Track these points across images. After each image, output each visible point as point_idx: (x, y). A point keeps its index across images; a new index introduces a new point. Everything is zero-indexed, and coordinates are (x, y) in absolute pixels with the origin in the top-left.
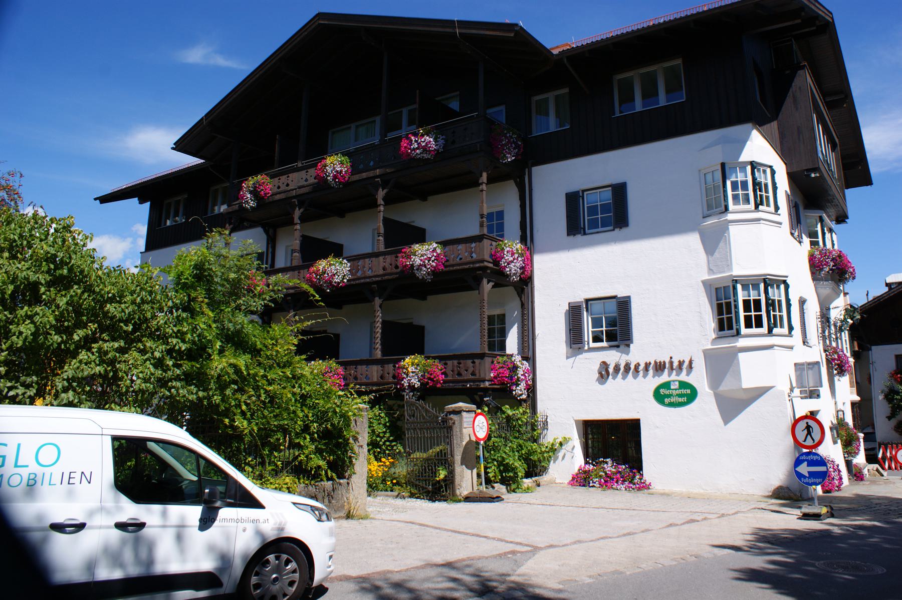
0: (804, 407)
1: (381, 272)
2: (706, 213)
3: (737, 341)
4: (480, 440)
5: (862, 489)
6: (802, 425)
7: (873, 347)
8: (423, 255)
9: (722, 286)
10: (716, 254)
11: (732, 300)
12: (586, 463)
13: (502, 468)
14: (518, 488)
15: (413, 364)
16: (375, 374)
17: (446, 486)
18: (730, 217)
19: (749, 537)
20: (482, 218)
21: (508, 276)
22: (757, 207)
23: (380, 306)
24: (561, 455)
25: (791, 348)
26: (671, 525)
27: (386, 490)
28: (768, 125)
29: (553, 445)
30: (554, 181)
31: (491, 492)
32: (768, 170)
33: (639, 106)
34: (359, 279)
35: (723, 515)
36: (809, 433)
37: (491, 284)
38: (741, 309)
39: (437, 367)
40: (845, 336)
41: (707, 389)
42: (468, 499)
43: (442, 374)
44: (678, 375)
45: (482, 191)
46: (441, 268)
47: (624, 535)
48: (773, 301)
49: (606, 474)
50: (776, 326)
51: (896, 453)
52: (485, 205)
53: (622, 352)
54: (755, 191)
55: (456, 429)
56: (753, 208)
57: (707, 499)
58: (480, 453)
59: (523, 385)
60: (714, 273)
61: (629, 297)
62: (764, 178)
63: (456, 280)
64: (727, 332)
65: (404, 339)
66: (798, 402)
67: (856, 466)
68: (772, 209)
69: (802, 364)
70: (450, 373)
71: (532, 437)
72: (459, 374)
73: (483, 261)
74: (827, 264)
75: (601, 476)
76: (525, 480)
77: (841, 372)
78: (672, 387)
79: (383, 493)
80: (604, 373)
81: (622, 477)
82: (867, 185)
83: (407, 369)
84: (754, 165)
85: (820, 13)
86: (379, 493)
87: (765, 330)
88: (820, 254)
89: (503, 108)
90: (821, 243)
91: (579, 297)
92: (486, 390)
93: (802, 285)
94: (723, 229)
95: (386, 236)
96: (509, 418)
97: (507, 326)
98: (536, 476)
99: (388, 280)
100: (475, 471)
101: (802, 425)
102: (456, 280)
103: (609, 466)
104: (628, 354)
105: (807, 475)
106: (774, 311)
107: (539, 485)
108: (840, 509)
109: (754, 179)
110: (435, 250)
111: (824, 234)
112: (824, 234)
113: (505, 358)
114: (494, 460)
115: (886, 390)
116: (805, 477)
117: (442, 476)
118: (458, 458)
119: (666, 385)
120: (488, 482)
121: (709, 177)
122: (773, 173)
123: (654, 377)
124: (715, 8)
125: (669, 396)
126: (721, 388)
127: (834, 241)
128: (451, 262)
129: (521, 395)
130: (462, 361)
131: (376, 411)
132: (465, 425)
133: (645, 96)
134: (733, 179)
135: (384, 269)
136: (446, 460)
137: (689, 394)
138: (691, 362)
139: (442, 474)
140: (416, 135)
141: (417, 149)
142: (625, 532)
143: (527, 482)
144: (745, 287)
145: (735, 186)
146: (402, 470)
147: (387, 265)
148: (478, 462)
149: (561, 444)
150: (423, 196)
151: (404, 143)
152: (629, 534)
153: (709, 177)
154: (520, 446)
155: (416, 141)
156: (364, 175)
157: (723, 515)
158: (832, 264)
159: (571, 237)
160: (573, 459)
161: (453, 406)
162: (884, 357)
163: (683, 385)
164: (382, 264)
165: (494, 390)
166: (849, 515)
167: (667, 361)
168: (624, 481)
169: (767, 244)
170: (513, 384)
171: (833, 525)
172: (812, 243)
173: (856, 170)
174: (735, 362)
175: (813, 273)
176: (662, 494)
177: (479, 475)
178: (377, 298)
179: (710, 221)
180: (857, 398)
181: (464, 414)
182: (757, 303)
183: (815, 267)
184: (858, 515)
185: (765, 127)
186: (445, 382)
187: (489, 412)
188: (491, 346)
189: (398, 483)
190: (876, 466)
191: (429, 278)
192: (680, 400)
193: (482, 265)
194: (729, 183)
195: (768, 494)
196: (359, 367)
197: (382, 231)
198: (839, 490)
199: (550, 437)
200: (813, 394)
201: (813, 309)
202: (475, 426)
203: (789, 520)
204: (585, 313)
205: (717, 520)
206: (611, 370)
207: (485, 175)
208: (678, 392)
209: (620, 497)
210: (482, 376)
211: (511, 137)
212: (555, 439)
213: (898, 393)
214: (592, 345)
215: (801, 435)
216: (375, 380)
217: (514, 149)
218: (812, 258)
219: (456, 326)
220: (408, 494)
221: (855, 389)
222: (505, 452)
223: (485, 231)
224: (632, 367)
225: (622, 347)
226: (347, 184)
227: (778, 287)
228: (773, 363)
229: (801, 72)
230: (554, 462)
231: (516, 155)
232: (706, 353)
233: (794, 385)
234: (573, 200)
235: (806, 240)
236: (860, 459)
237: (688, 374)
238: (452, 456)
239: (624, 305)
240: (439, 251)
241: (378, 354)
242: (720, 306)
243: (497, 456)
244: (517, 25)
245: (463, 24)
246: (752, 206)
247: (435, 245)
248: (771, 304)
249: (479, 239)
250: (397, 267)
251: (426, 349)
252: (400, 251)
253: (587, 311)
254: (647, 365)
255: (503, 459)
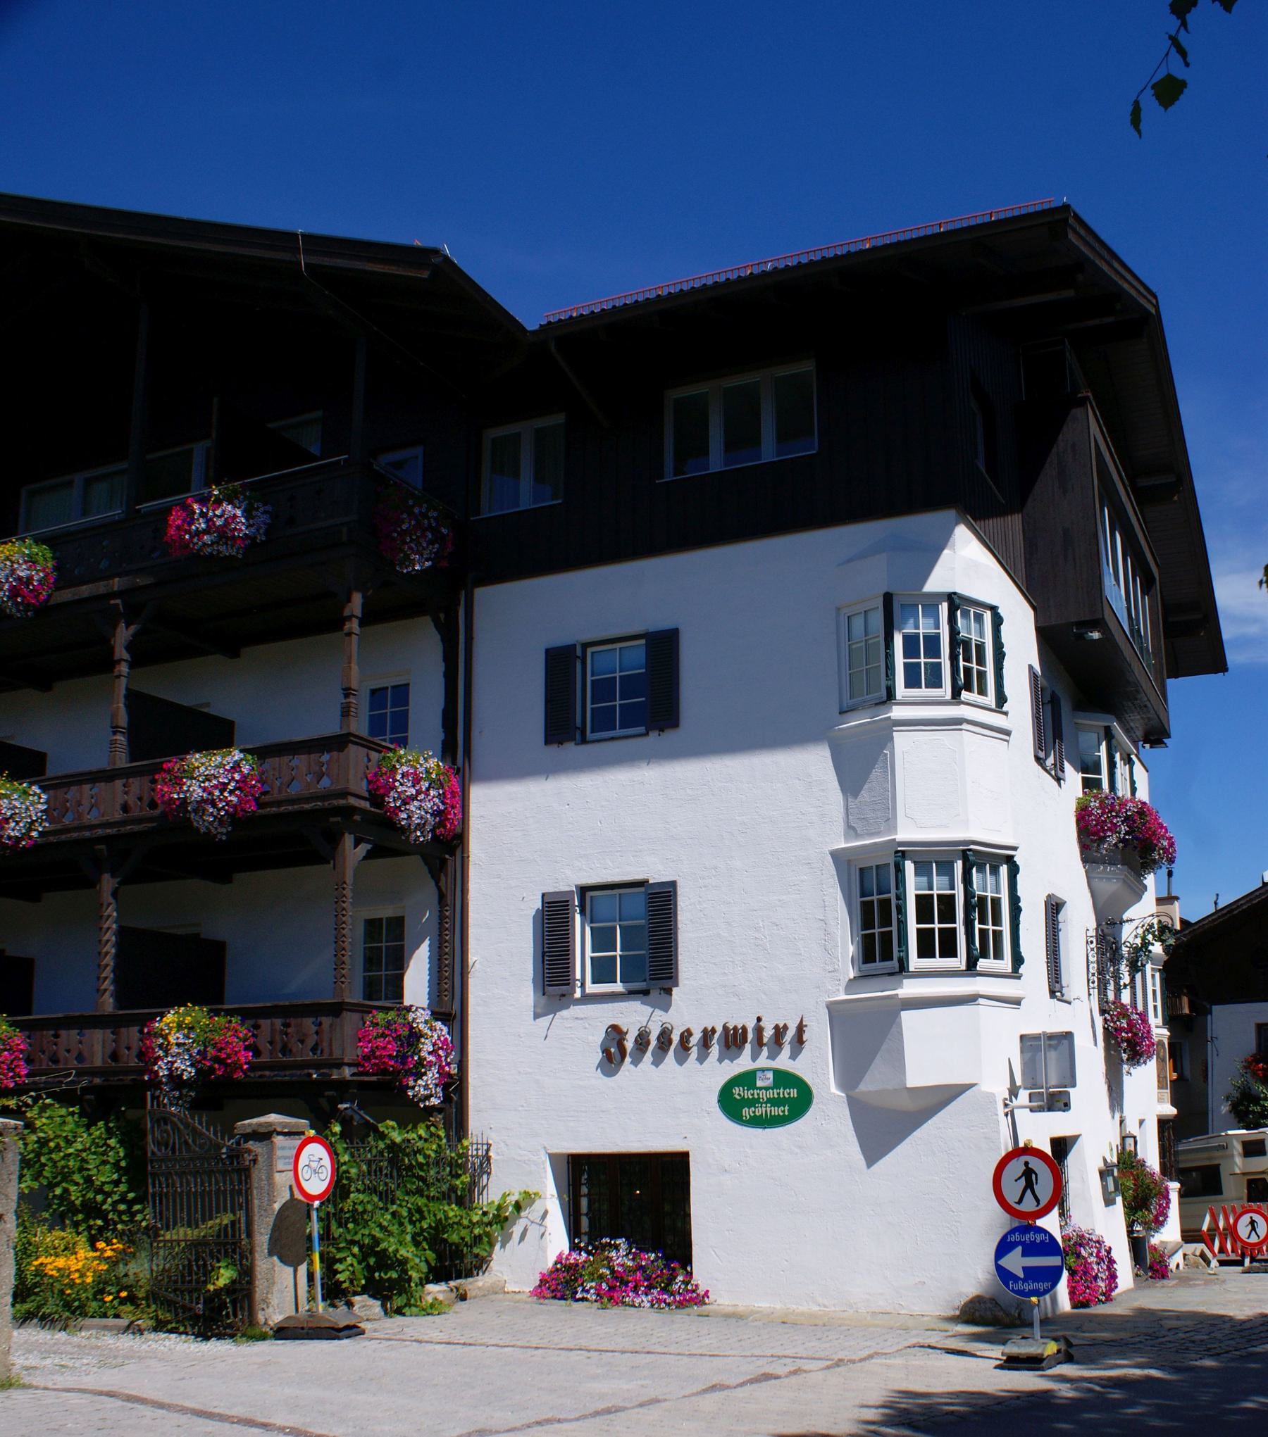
0: (1039, 1130)
1: (118, 816)
2: (847, 702)
3: (900, 985)
4: (314, 1198)
5: (1160, 1298)
6: (1016, 1167)
7: (1215, 1009)
8: (210, 777)
9: (873, 863)
10: (864, 793)
11: (893, 896)
12: (574, 1247)
13: (372, 1261)
14: (408, 1305)
15: (180, 1027)
16: (98, 1048)
17: (234, 1302)
18: (897, 712)
19: (871, 1414)
20: (347, 696)
21: (403, 830)
22: (956, 694)
23: (115, 894)
24: (517, 1230)
25: (1017, 1002)
26: (713, 1388)
27: (105, 1316)
28: (998, 522)
29: (499, 1208)
30: (523, 620)
31: (339, 1315)
32: (988, 616)
33: (716, 461)
34: (67, 830)
35: (839, 1363)
36: (1030, 1185)
37: (364, 848)
38: (917, 914)
39: (231, 1032)
40: (1152, 981)
41: (834, 1089)
42: (283, 1332)
43: (247, 1048)
44: (772, 1056)
45: (349, 634)
46: (251, 808)
47: (597, 1414)
48: (982, 899)
49: (613, 1272)
50: (984, 954)
51: (1236, 1221)
52: (355, 667)
53: (654, 1006)
54: (954, 658)
55: (258, 1175)
56: (948, 696)
57: (818, 1325)
58: (315, 1227)
59: (431, 1076)
60: (858, 836)
61: (673, 884)
62: (978, 632)
63: (284, 837)
64: (879, 965)
65: (174, 968)
66: (1023, 1116)
67: (1154, 1248)
68: (990, 699)
69: (1036, 1038)
70: (265, 1047)
71: (453, 1189)
72: (285, 1050)
73: (345, 794)
74: (1114, 828)
75: (601, 1277)
76: (431, 1287)
77: (1136, 1056)
78: (759, 1084)
79: (97, 1321)
80: (615, 1051)
81: (648, 1278)
82: (1216, 672)
83: (165, 1037)
84: (956, 602)
85: (1126, 286)
86: (88, 1321)
87: (960, 962)
88: (1102, 806)
89: (418, 451)
90: (1105, 785)
91: (567, 880)
92: (343, 1085)
93: (1053, 864)
94: (882, 737)
95: (133, 733)
96: (393, 1146)
97: (407, 942)
98: (459, 1277)
99: (133, 835)
100: (303, 1269)
101: (1016, 1167)
102: (284, 837)
103: (621, 1256)
104: (666, 1008)
105: (1022, 1276)
106: (983, 921)
107: (463, 1298)
108: (1093, 1344)
109: (954, 632)
110: (236, 767)
111: (1112, 765)
112: (1112, 765)
113: (391, 1015)
114: (353, 1242)
115: (1236, 1094)
116: (1015, 1278)
117: (221, 1282)
118: (262, 1239)
119: (747, 1079)
120: (334, 1292)
121: (858, 623)
122: (998, 621)
123: (720, 1060)
124: (885, 246)
125: (752, 1102)
126: (863, 1087)
127: (1137, 782)
128: (276, 795)
129: (428, 1097)
130: (293, 1021)
131: (99, 1130)
132: (280, 1165)
133: (731, 445)
134: (909, 630)
135: (125, 808)
136: (236, 1245)
137: (794, 1100)
138: (801, 1029)
139: (225, 1276)
140: (203, 501)
141: (205, 532)
142: (601, 1406)
143: (436, 1290)
144: (922, 869)
145: (911, 645)
146: (140, 1269)
147: (131, 800)
148: (310, 1249)
149: (518, 1207)
150: (231, 646)
151: (176, 519)
152: (608, 1411)
153: (858, 623)
154: (419, 1210)
155: (203, 515)
156: (85, 590)
157: (839, 1363)
158: (1124, 828)
159: (554, 748)
160: (548, 1238)
161: (255, 1121)
162: (1235, 1028)
163: (784, 1078)
164: (121, 798)
165: (363, 1086)
166: (1106, 1356)
167: (751, 1025)
168: (650, 1287)
169: (981, 777)
170: (409, 1073)
171: (1061, 1380)
172: (1087, 784)
173: (1193, 637)
174: (894, 1029)
175: (1084, 848)
176: (728, 1316)
177: (311, 1277)
178: (106, 876)
179: (854, 722)
180: (1170, 1110)
181: (279, 1140)
182: (947, 902)
183: (1089, 834)
184: (1123, 1355)
185: (990, 523)
186: (253, 1067)
187: (343, 1135)
188: (371, 990)
189: (132, 1299)
190: (1201, 1247)
191: (222, 833)
192: (776, 1111)
193: (342, 802)
194: (898, 640)
195: (951, 1313)
196: (63, 1033)
197: (123, 720)
198: (1109, 1299)
199: (497, 1189)
200: (1057, 1102)
201: (1080, 921)
202: (308, 1166)
203: (981, 1373)
204: (578, 917)
205: (821, 1375)
206: (629, 1044)
207: (357, 599)
208: (770, 1094)
209: (641, 1323)
210: (337, 1054)
211: (424, 515)
212: (505, 1196)
213: (1256, 1100)
214: (591, 988)
215: (1012, 1190)
216: (98, 1062)
217: (431, 542)
218: (1083, 815)
219: (289, 939)
220: (151, 1323)
221: (1167, 1093)
222: (380, 1226)
223: (360, 725)
224: (676, 1038)
225: (654, 994)
226: (44, 610)
227: (995, 871)
228: (965, 1036)
229: (1077, 412)
230: (503, 1246)
231: (436, 558)
232: (834, 1010)
233: (1019, 1082)
234: (561, 664)
235: (1073, 778)
236: (1169, 1233)
237: (794, 1056)
238: (250, 1234)
239: (659, 903)
240: (246, 769)
241: (108, 1004)
242: (867, 909)
243: (362, 1235)
244: (436, 252)
245: (316, 243)
246: (946, 691)
247: (237, 755)
248: (976, 905)
249: (339, 742)
250: (153, 805)
251: (229, 990)
252: (158, 769)
253: (583, 912)
254: (708, 1035)
255: (377, 1242)
